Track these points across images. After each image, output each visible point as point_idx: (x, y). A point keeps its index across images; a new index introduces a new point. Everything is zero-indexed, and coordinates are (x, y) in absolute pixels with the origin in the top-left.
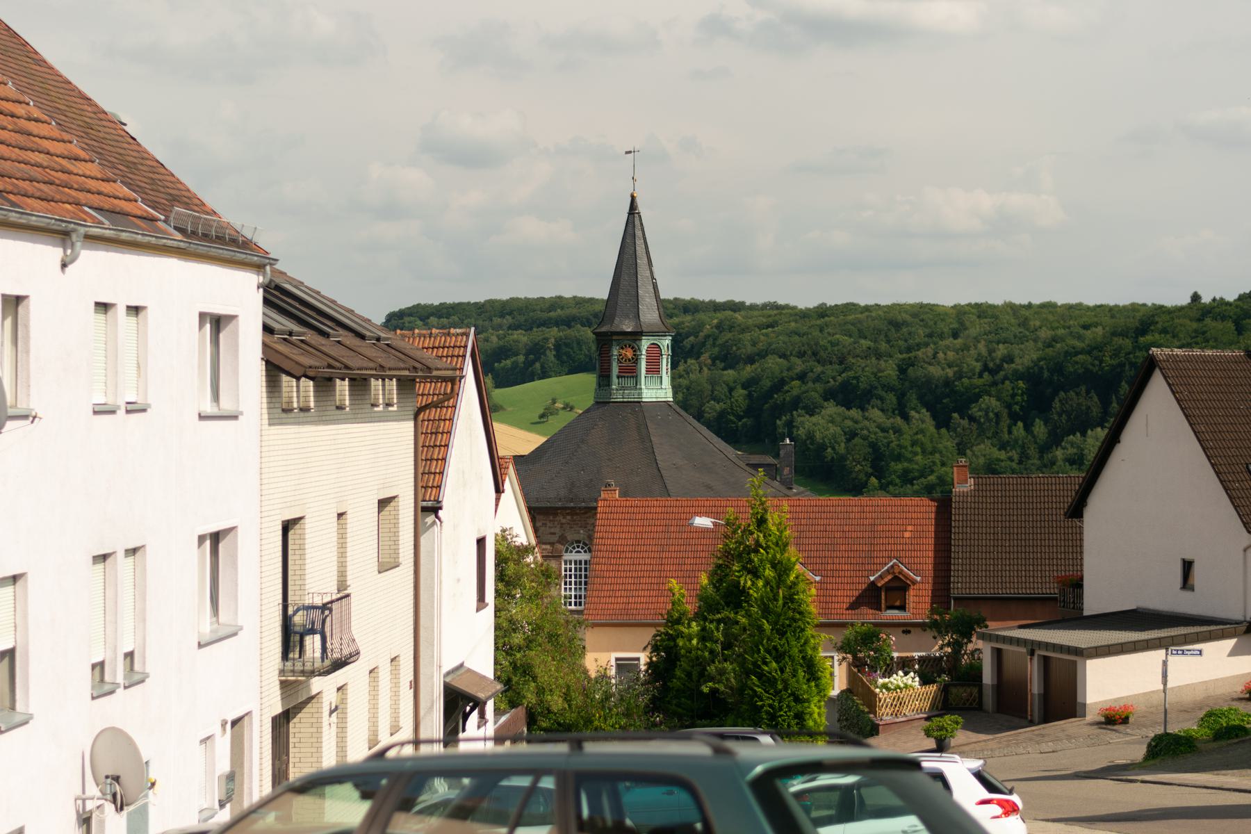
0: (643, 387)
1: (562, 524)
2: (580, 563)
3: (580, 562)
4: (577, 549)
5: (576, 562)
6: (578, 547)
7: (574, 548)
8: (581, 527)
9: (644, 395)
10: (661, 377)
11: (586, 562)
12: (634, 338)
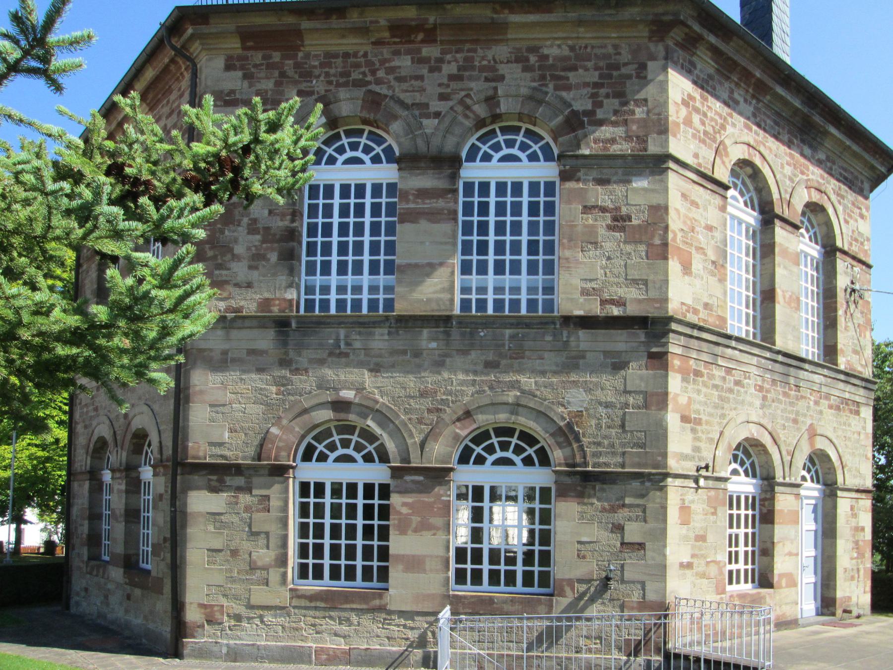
6: (354, 147)
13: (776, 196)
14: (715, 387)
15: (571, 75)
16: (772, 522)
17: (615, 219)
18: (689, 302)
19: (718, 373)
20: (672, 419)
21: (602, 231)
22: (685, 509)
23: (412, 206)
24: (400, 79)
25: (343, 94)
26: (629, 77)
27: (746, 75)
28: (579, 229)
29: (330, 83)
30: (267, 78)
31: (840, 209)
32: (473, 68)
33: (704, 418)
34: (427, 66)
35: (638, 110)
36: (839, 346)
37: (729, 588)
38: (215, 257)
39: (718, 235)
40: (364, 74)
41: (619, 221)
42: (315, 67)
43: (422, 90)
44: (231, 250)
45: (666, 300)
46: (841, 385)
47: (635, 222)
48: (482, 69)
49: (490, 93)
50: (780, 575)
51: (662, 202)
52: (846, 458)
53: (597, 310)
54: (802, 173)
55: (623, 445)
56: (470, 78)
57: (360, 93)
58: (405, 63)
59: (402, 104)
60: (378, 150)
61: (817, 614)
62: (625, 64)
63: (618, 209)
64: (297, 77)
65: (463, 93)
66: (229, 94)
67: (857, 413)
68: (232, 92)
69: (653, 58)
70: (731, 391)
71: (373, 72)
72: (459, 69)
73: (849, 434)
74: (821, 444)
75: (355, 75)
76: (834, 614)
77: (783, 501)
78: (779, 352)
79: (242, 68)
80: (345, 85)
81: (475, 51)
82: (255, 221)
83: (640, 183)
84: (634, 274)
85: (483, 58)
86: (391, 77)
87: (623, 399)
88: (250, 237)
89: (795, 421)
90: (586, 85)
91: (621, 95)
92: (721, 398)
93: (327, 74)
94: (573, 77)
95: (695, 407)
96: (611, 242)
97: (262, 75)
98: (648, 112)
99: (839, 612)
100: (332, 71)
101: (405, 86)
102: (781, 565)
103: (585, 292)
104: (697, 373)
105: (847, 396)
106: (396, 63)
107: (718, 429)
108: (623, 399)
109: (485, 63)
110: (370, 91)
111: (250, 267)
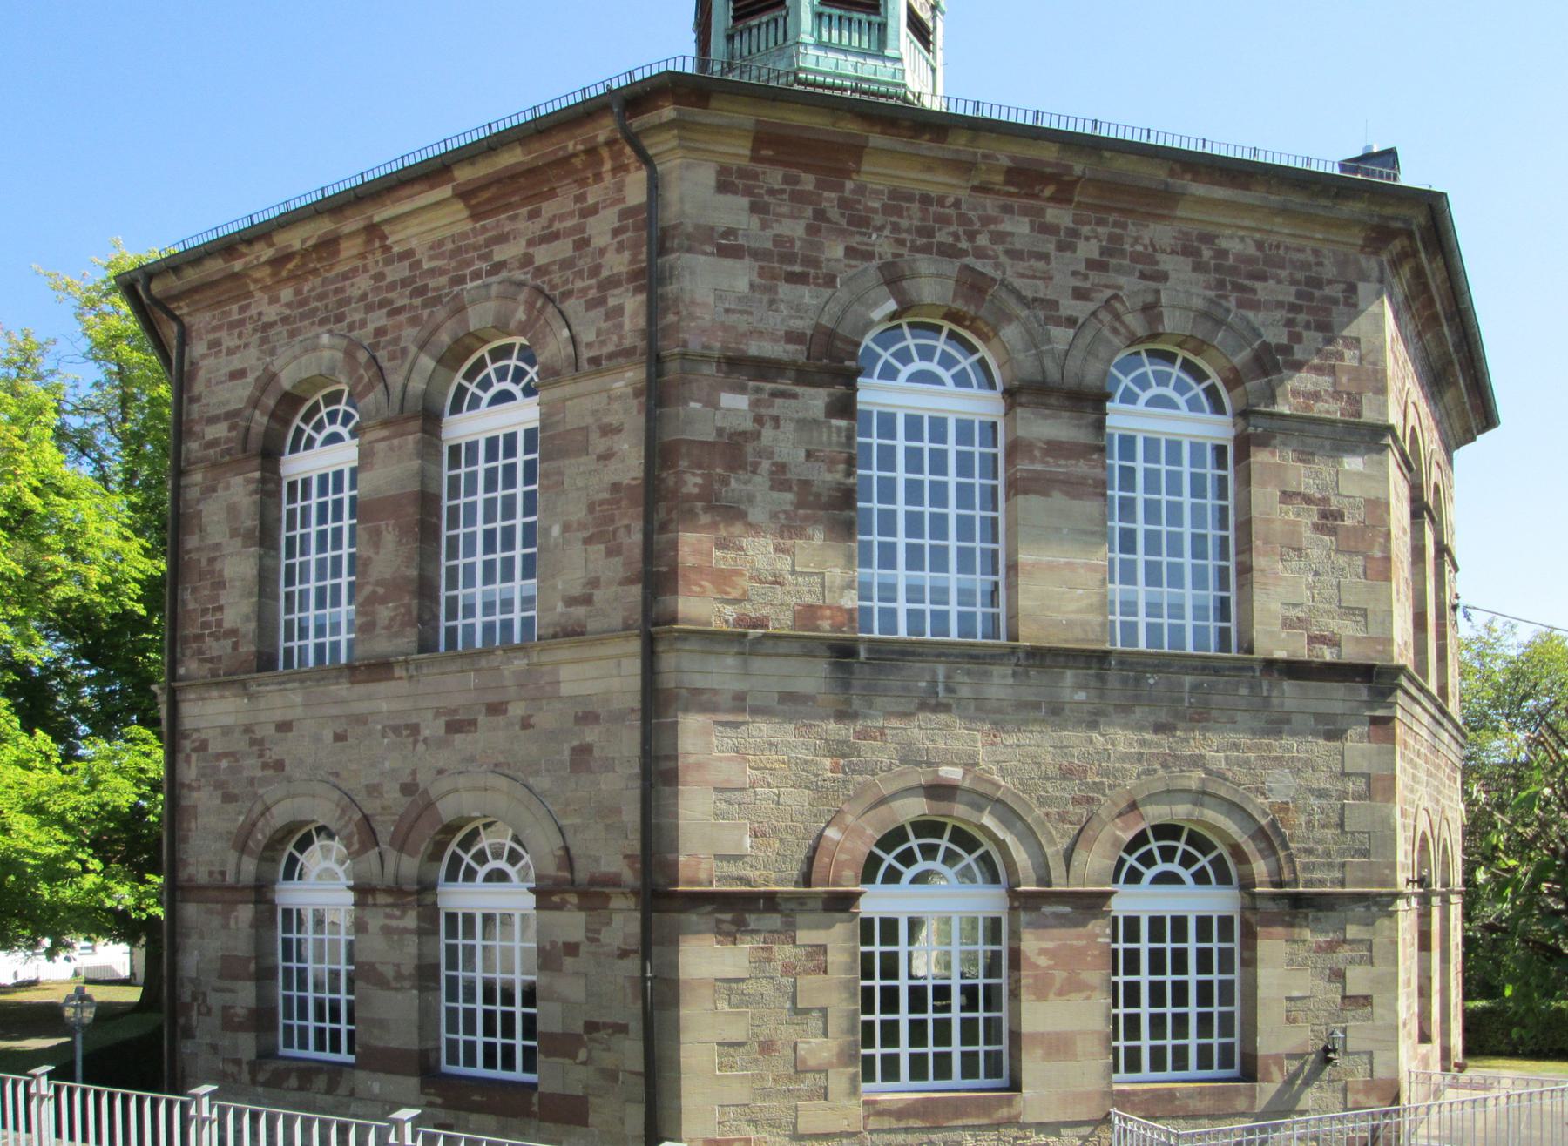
1: (268, 326)
6: (926, 353)
7: (904, 356)
8: (323, 322)
10: (883, 27)
11: (1197, 449)
15: (1258, 285)
23: (1039, 467)
24: (1014, 255)
25: (924, 264)
26: (1335, 302)
28: (1277, 526)
30: (792, 216)
32: (1122, 253)
34: (1053, 239)
35: (1348, 353)
41: (1329, 519)
42: (874, 211)
43: (1047, 278)
47: (1348, 522)
48: (1136, 258)
49: (1150, 298)
51: (1381, 495)
56: (1119, 270)
57: (952, 267)
58: (1019, 227)
62: (1330, 282)
63: (1326, 500)
64: (843, 222)
65: (1108, 293)
68: (730, 232)
69: (1365, 278)
71: (972, 236)
75: (942, 237)
79: (748, 192)
80: (926, 249)
81: (1124, 226)
82: (782, 467)
83: (1353, 463)
86: (999, 248)
87: (1340, 786)
93: (896, 228)
94: (1263, 290)
96: (1319, 548)
97: (785, 210)
101: (1021, 266)
103: (1288, 623)
106: (1007, 226)
108: (1340, 786)
109: (1139, 248)
110: (966, 267)
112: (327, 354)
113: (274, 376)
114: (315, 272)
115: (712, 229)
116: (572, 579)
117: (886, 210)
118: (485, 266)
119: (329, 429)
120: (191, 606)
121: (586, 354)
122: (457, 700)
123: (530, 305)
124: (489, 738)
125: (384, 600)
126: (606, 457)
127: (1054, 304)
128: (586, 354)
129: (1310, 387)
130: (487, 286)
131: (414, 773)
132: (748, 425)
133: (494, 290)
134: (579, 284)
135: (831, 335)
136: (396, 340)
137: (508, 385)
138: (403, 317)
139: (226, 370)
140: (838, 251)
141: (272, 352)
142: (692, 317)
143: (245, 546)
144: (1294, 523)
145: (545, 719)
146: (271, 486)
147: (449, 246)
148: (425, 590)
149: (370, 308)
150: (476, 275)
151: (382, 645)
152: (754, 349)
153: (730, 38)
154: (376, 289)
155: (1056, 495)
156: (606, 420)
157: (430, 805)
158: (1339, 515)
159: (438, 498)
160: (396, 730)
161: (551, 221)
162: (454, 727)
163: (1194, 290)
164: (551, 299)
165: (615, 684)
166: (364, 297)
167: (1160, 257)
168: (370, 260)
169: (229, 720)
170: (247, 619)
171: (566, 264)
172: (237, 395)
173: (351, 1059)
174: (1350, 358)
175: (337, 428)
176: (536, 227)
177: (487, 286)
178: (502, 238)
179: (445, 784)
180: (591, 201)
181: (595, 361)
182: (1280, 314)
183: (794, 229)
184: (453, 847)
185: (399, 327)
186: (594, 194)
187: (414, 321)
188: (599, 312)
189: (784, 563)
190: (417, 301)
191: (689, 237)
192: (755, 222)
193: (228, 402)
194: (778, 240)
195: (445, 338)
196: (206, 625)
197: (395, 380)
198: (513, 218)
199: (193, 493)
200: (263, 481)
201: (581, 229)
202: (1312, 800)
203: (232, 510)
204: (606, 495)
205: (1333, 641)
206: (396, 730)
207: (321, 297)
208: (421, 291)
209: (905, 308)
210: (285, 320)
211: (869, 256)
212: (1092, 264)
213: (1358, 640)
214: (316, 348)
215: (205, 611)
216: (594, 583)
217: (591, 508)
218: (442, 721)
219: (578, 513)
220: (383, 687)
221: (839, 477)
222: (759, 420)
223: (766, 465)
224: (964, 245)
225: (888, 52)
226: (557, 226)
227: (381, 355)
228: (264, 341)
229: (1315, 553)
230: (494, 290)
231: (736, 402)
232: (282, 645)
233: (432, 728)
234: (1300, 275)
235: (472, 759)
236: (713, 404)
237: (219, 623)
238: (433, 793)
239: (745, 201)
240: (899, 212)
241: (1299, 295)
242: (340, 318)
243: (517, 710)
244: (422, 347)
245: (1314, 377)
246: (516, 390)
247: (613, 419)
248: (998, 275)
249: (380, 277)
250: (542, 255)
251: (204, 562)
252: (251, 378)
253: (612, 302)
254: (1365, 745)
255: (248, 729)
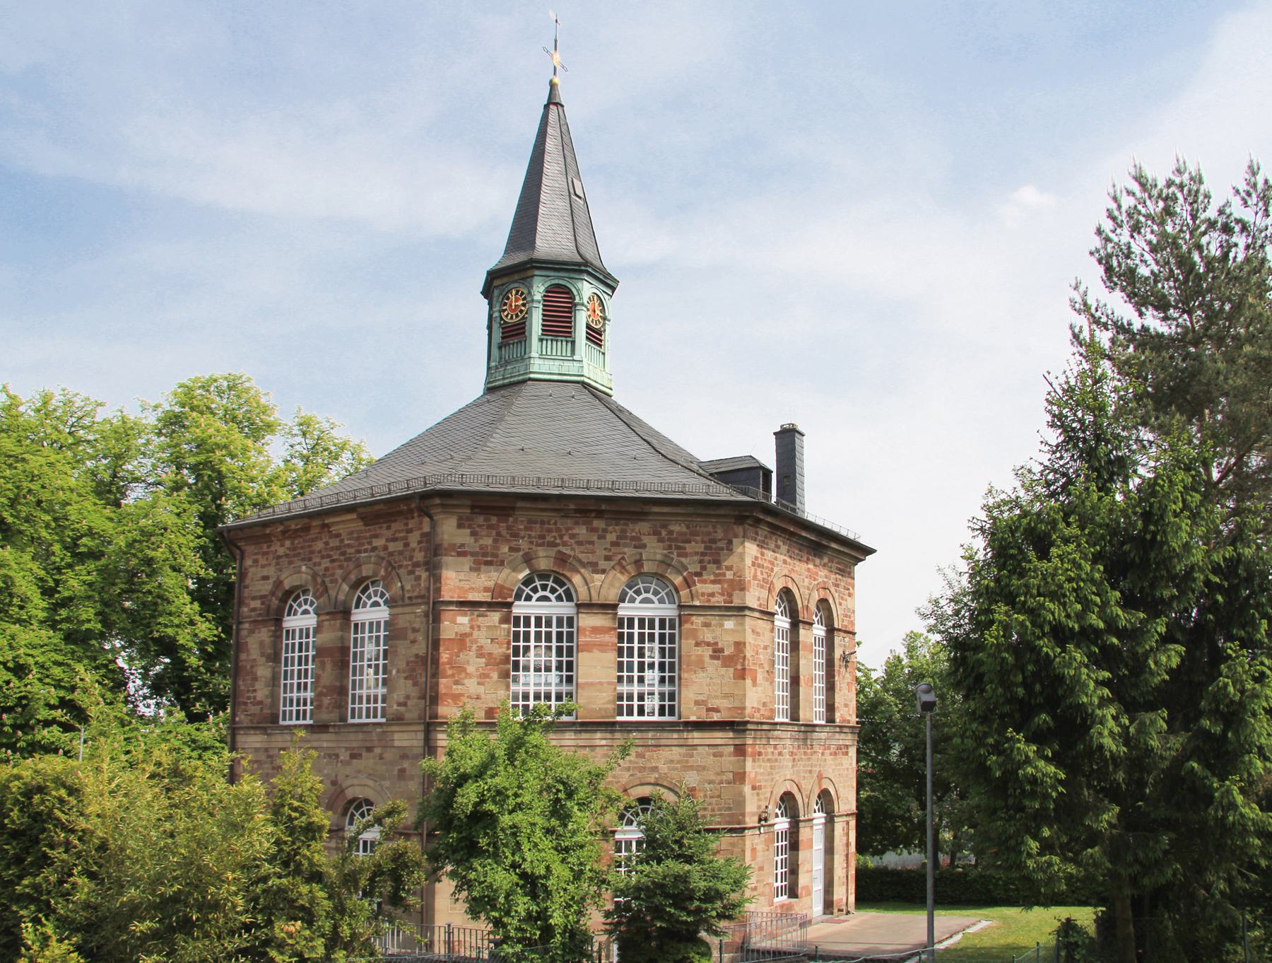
0: (534, 354)
1: (279, 557)
2: (549, 624)
3: (652, 621)
4: (541, 593)
5: (642, 621)
6: (544, 588)
7: (535, 590)
8: (303, 560)
9: (534, 368)
10: (573, 343)
11: (662, 622)
12: (523, 275)
13: (800, 606)
14: (769, 760)
15: (687, 545)
16: (797, 849)
17: (714, 651)
18: (755, 706)
19: (770, 749)
20: (747, 789)
21: (707, 659)
22: (754, 850)
23: (589, 639)
24: (580, 543)
25: (541, 552)
26: (722, 549)
27: (785, 531)
28: (693, 658)
29: (531, 543)
30: (488, 536)
31: (836, 595)
32: (626, 538)
33: (762, 784)
34: (596, 534)
35: (728, 573)
36: (836, 705)
37: (776, 900)
38: (453, 676)
39: (769, 650)
40: (555, 537)
41: (717, 652)
42: (520, 530)
43: (593, 552)
44: (464, 670)
45: (744, 708)
46: (837, 736)
47: (726, 653)
48: (633, 539)
49: (638, 557)
50: (803, 888)
51: (742, 640)
52: (841, 791)
53: (704, 717)
54: (815, 580)
55: (720, 809)
56: (625, 545)
57: (552, 552)
58: (581, 531)
59: (580, 561)
60: (561, 591)
61: (824, 914)
62: (720, 540)
63: (716, 644)
64: (508, 536)
65: (620, 556)
66: (460, 547)
67: (847, 753)
68: (463, 545)
69: (736, 536)
70: (776, 760)
71: (561, 537)
72: (618, 537)
73: (841, 772)
74: (826, 785)
75: (549, 538)
76: (832, 913)
77: (804, 833)
78: (803, 725)
79: (470, 527)
80: (542, 545)
81: (627, 525)
82: (481, 647)
83: (729, 624)
84: (727, 690)
85: (633, 531)
86: (573, 541)
87: (719, 778)
88: (478, 660)
89: (810, 772)
90: (696, 553)
91: (717, 562)
92: (771, 767)
93: (530, 536)
94: (689, 548)
95: (759, 777)
96: (713, 666)
97: (484, 533)
98: (734, 574)
99: (835, 911)
100: (533, 534)
101: (582, 548)
102: (803, 880)
103: (697, 703)
104: (760, 754)
105: (841, 743)
106: (576, 531)
107: (769, 790)
108: (719, 778)
109: (634, 534)
110: (560, 552)
111: (479, 683)
112: (304, 575)
113: (281, 582)
114: (300, 536)
115: (455, 545)
116: (398, 696)
117: (526, 529)
118: (369, 547)
119: (304, 607)
120: (242, 688)
121: (407, 595)
122: (355, 745)
123: (386, 570)
124: (367, 761)
125: (326, 695)
126: (413, 642)
127: (596, 564)
128: (407, 595)
129: (710, 591)
130: (370, 557)
131: (336, 776)
132: (468, 630)
133: (373, 559)
134: (405, 563)
135: (502, 587)
136: (333, 575)
137: (378, 599)
138: (336, 564)
139: (260, 575)
140: (506, 549)
141: (281, 570)
142: (446, 584)
143: (267, 662)
144: (701, 656)
145: (389, 755)
146: (278, 633)
147: (355, 535)
148: (342, 691)
149: (323, 557)
150: (366, 551)
151: (325, 716)
152: (472, 597)
153: (500, 348)
154: (326, 549)
155: (595, 651)
156: (414, 625)
157: (343, 791)
158: (722, 650)
159: (349, 648)
160: (330, 756)
161: (396, 531)
162: (353, 756)
163: (658, 551)
164: (394, 568)
165: (415, 743)
166: (320, 552)
167: (643, 537)
168: (323, 535)
169: (258, 745)
170: (267, 697)
171: (401, 553)
172: (266, 588)
173: (384, 720)
174: (729, 575)
175: (307, 607)
176: (389, 534)
177: (370, 557)
178: (376, 536)
179: (349, 782)
180: (410, 526)
181: (410, 598)
182: (696, 558)
183: (488, 541)
184: (351, 810)
185: (334, 568)
186: (412, 524)
187: (341, 567)
188: (412, 576)
189: (481, 689)
190: (342, 558)
191: (446, 549)
192: (472, 540)
193: (260, 590)
194: (481, 547)
195: (353, 577)
196: (249, 698)
197: (333, 593)
198: (381, 528)
199: (244, 633)
200: (275, 631)
201: (406, 538)
202: (706, 785)
203: (261, 643)
204: (413, 659)
205: (717, 710)
206: (330, 756)
207: (302, 548)
208: (343, 554)
209: (533, 571)
210: (287, 556)
211: (518, 550)
212: (614, 544)
213: (730, 709)
214: (300, 572)
215: (248, 691)
216: (408, 697)
217: (408, 663)
218: (349, 752)
219: (403, 665)
220: (324, 736)
221: (504, 650)
222: (472, 627)
223: (474, 647)
224: (558, 541)
225: (576, 357)
226: (398, 535)
227: (327, 580)
228: (277, 564)
229: (710, 669)
230: (373, 559)
231: (463, 620)
232: (282, 708)
233: (344, 756)
234: (706, 539)
235: (359, 772)
236: (454, 622)
237: (255, 697)
238: (344, 786)
239: (468, 531)
240: (531, 529)
241: (706, 548)
242: (310, 559)
243: (378, 751)
244: (344, 580)
245: (712, 586)
246: (381, 601)
247: (417, 626)
248: (572, 553)
249: (327, 543)
250: (392, 547)
251: (248, 667)
252: (271, 581)
253: (417, 573)
254: (733, 758)
255: (266, 750)
